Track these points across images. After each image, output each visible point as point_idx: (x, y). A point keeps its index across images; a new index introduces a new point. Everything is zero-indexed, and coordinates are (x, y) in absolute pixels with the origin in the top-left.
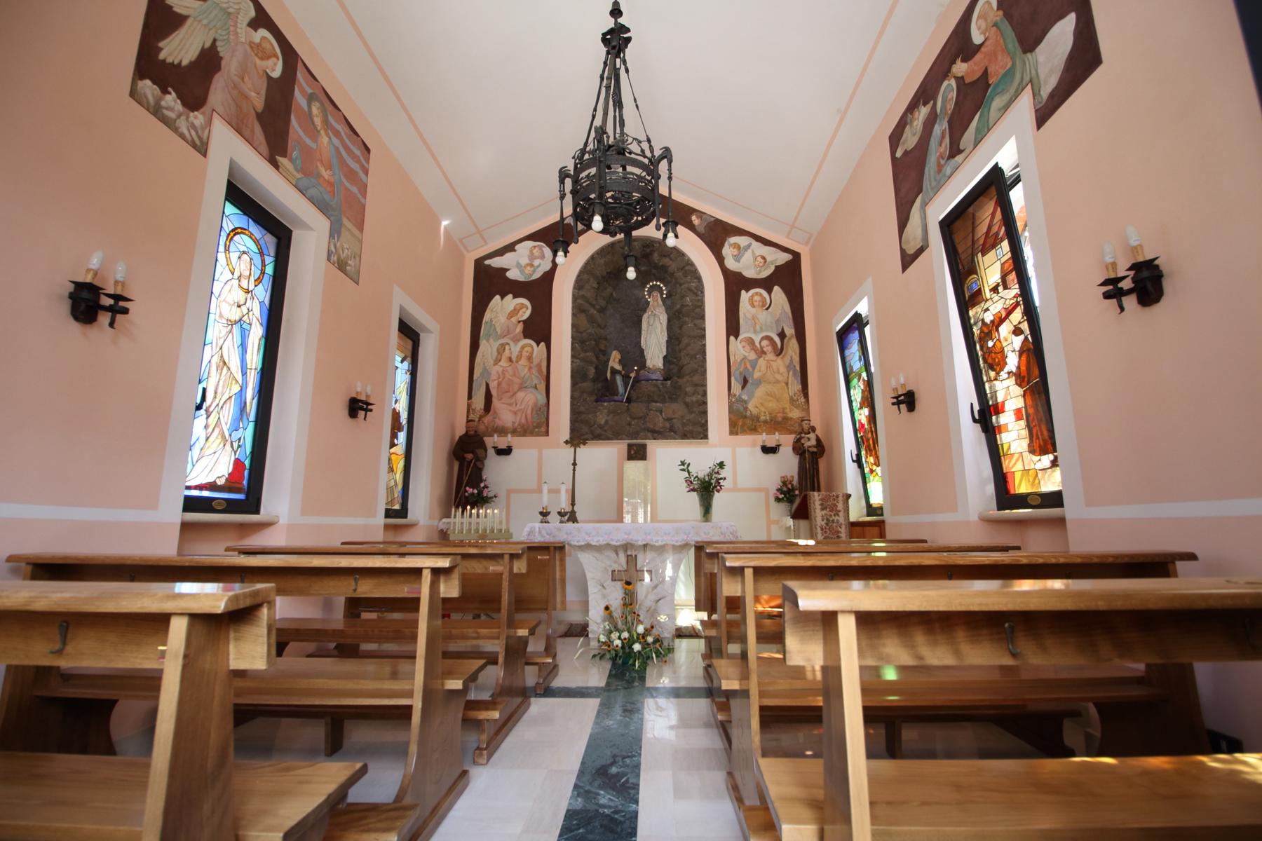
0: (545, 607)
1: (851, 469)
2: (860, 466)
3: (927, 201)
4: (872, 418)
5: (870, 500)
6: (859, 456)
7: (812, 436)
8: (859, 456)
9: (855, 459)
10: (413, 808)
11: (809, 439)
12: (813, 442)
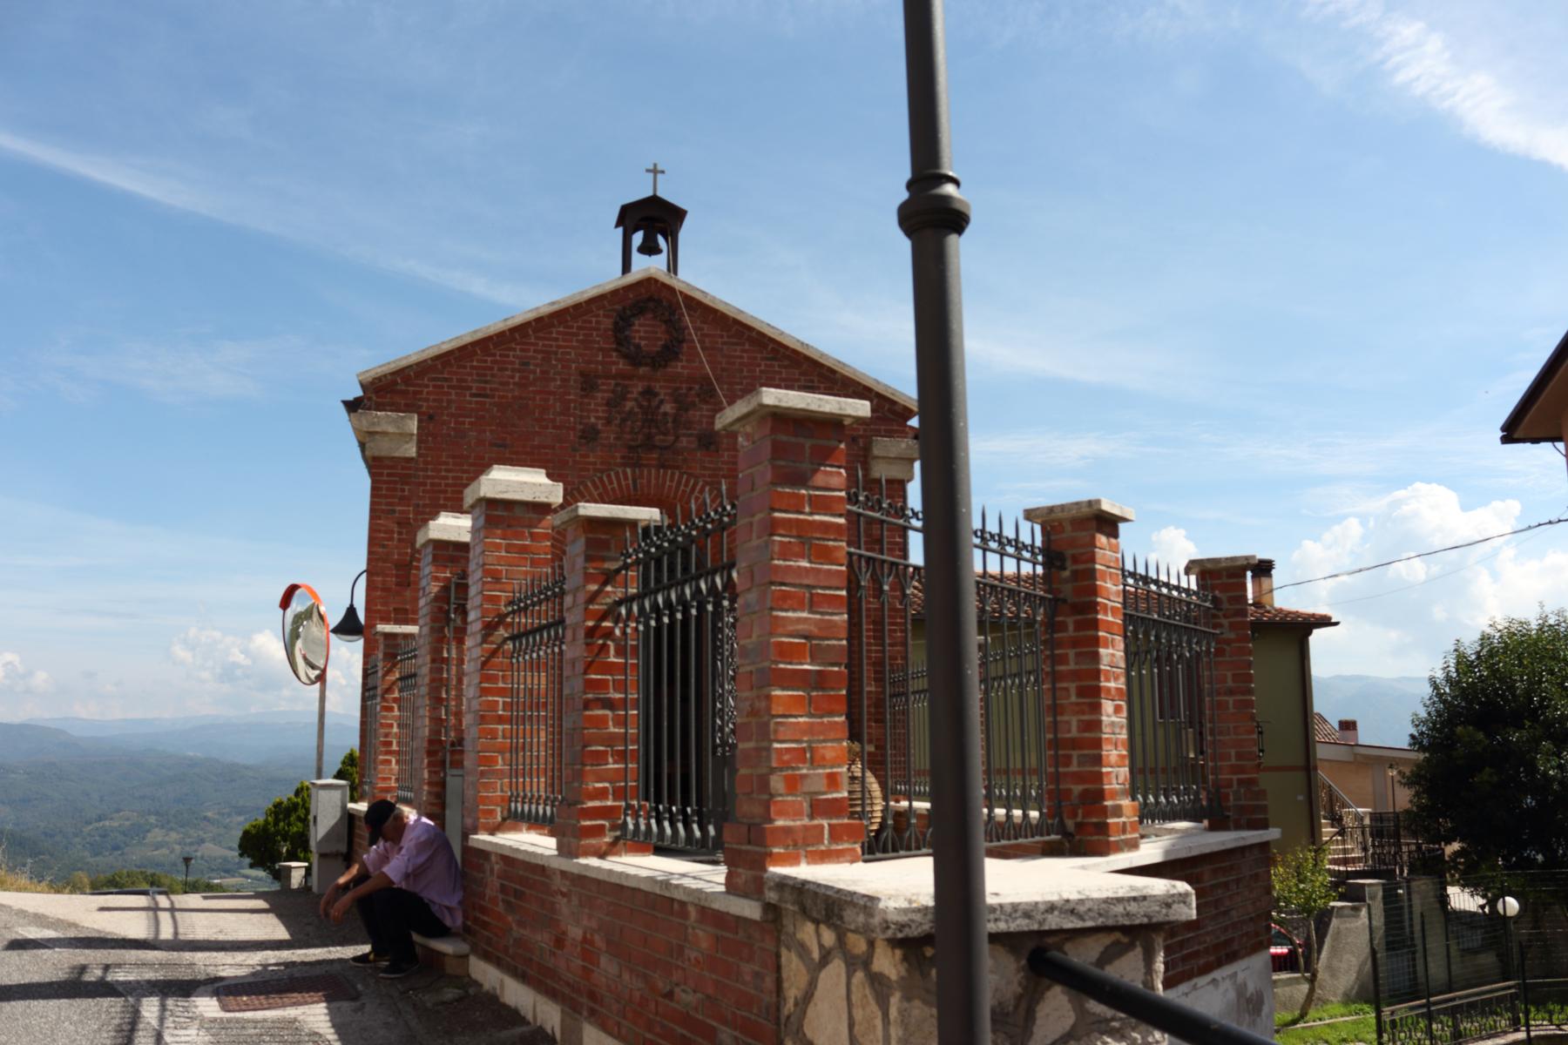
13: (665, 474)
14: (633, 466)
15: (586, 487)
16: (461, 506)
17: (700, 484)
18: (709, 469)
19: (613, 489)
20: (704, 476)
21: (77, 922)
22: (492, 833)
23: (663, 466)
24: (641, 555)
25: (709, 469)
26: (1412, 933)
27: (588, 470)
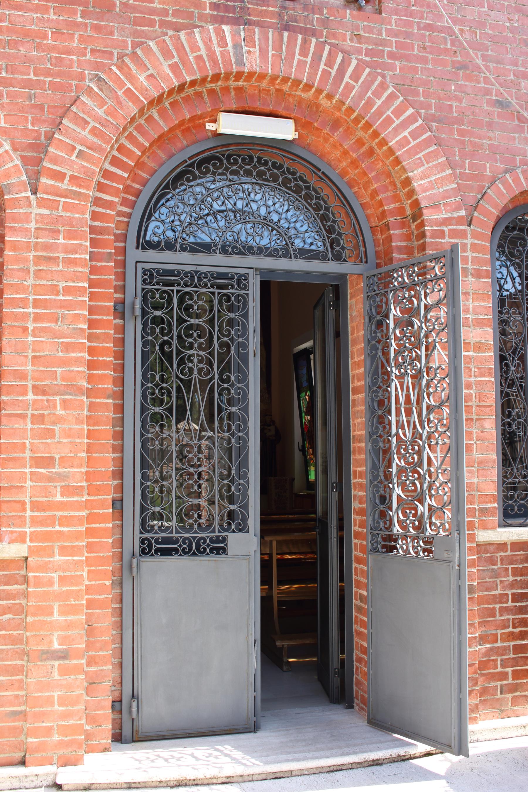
0: (5, 154)
1: (297, 456)
2: (304, 454)
3: (494, 546)
4: (313, 421)
5: (440, 773)
6: (303, 446)
7: (272, 428)
8: (303, 446)
9: (301, 448)
10: (506, 213)
11: (270, 430)
12: (273, 432)
13: (292, 41)
14: (235, 22)
15: (148, 51)
16: (260, 272)
17: (354, 63)
18: (368, 41)
19: (199, 58)
20: (359, 51)
21: (368, 728)
22: (73, 706)
23: (286, 27)
24: (395, 275)
25: (368, 41)
26: (326, 513)
27: (151, 23)
